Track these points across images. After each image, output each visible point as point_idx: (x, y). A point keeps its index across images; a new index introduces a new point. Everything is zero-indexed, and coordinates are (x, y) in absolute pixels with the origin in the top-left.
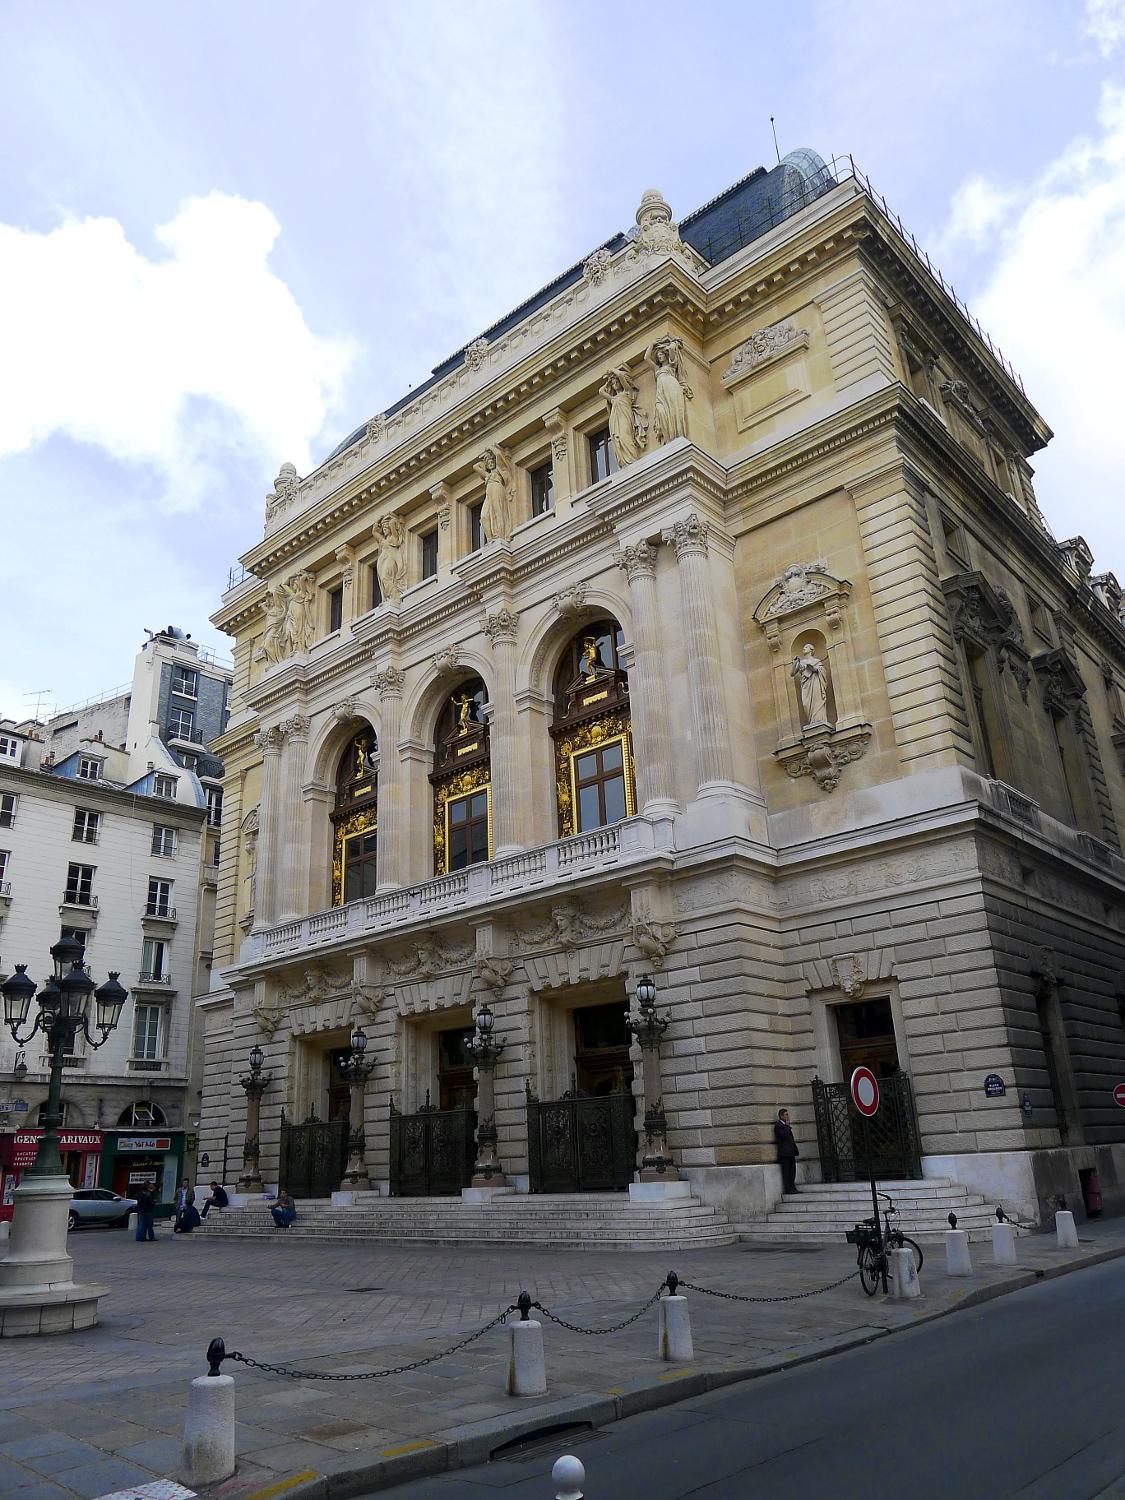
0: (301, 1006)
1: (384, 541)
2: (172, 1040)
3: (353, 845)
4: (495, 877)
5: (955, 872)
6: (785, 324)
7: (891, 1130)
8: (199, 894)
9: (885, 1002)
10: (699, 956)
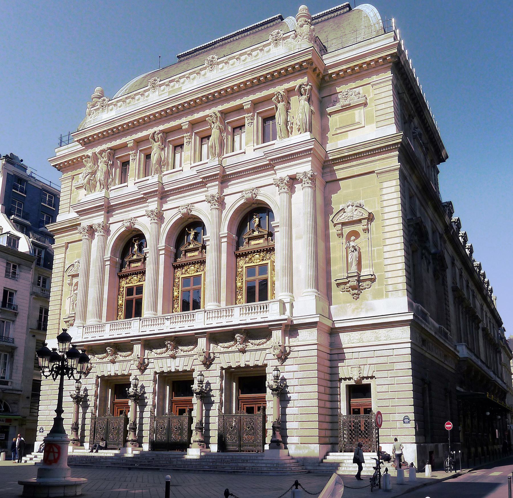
0: (103, 363)
1: (155, 144)
2: (14, 371)
3: (130, 291)
4: (209, 316)
5: (401, 338)
6: (357, 90)
7: (367, 434)
8: (30, 300)
9: (368, 386)
10: (299, 361)
